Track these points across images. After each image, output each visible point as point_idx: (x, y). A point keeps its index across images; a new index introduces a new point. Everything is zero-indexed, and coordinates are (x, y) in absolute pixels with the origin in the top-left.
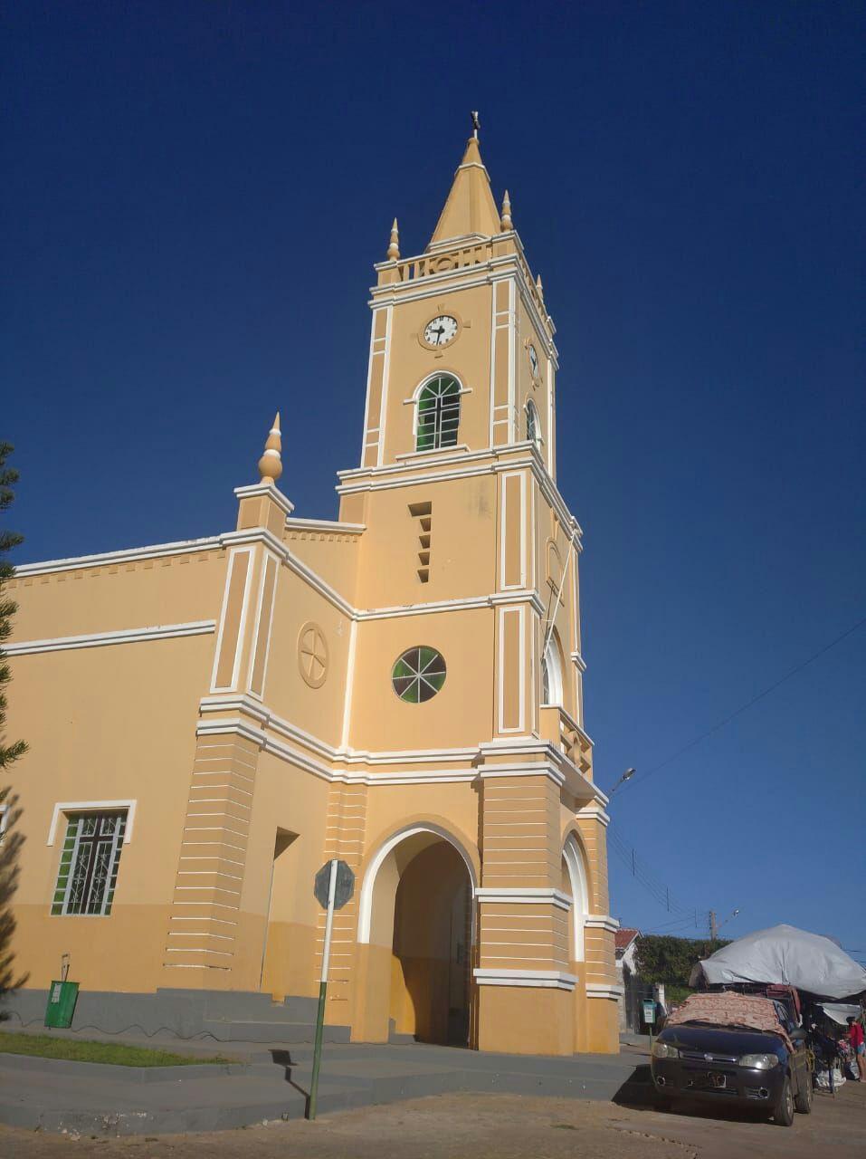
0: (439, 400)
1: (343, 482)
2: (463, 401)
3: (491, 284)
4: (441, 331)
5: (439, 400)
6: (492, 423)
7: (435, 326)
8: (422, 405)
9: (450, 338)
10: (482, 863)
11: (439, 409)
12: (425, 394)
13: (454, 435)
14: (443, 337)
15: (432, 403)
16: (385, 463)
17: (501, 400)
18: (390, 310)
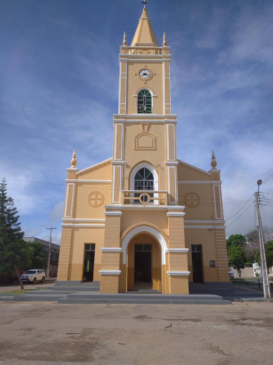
5: (145, 97)
13: (150, 110)
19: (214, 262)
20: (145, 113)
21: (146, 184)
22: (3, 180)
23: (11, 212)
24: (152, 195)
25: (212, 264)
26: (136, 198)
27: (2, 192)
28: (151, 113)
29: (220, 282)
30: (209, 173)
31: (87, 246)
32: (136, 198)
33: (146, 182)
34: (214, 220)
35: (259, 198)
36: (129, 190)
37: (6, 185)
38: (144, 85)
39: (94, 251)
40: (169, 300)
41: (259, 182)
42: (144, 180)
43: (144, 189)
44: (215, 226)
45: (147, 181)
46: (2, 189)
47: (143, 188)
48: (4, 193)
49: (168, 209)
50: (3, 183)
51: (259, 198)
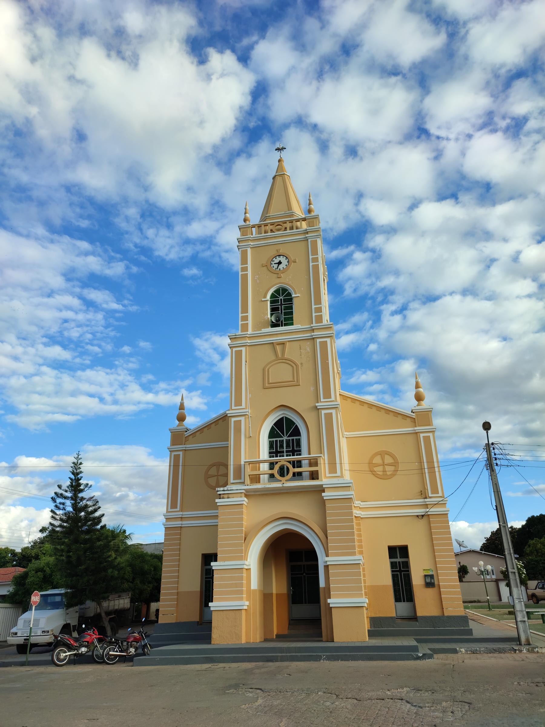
0: (281, 299)
1: (315, 331)
2: (295, 301)
3: (306, 240)
4: (280, 263)
5: (281, 299)
6: (240, 323)
7: (277, 261)
8: (272, 302)
9: (285, 267)
10: (327, 538)
11: (281, 305)
12: (273, 296)
13: (292, 319)
14: (281, 267)
15: (277, 301)
16: (253, 331)
17: (245, 309)
18: (249, 250)
19: (432, 576)
20: (282, 326)
21: (288, 446)
22: (76, 456)
23: (90, 509)
24: (299, 464)
25: (428, 580)
26: (297, 470)
27: (75, 477)
28: (292, 324)
29: (446, 614)
30: (412, 414)
31: (393, 551)
32: (297, 470)
33: (288, 442)
34: (426, 498)
35: (495, 454)
36: (310, 454)
37: (81, 464)
38: (278, 280)
39: (394, 560)
40: (320, 654)
41: (487, 427)
42: (285, 438)
43: (285, 454)
44: (427, 510)
45: (290, 440)
46: (75, 471)
47: (283, 452)
48: (78, 478)
49: (324, 486)
50: (76, 461)
51: (495, 454)
